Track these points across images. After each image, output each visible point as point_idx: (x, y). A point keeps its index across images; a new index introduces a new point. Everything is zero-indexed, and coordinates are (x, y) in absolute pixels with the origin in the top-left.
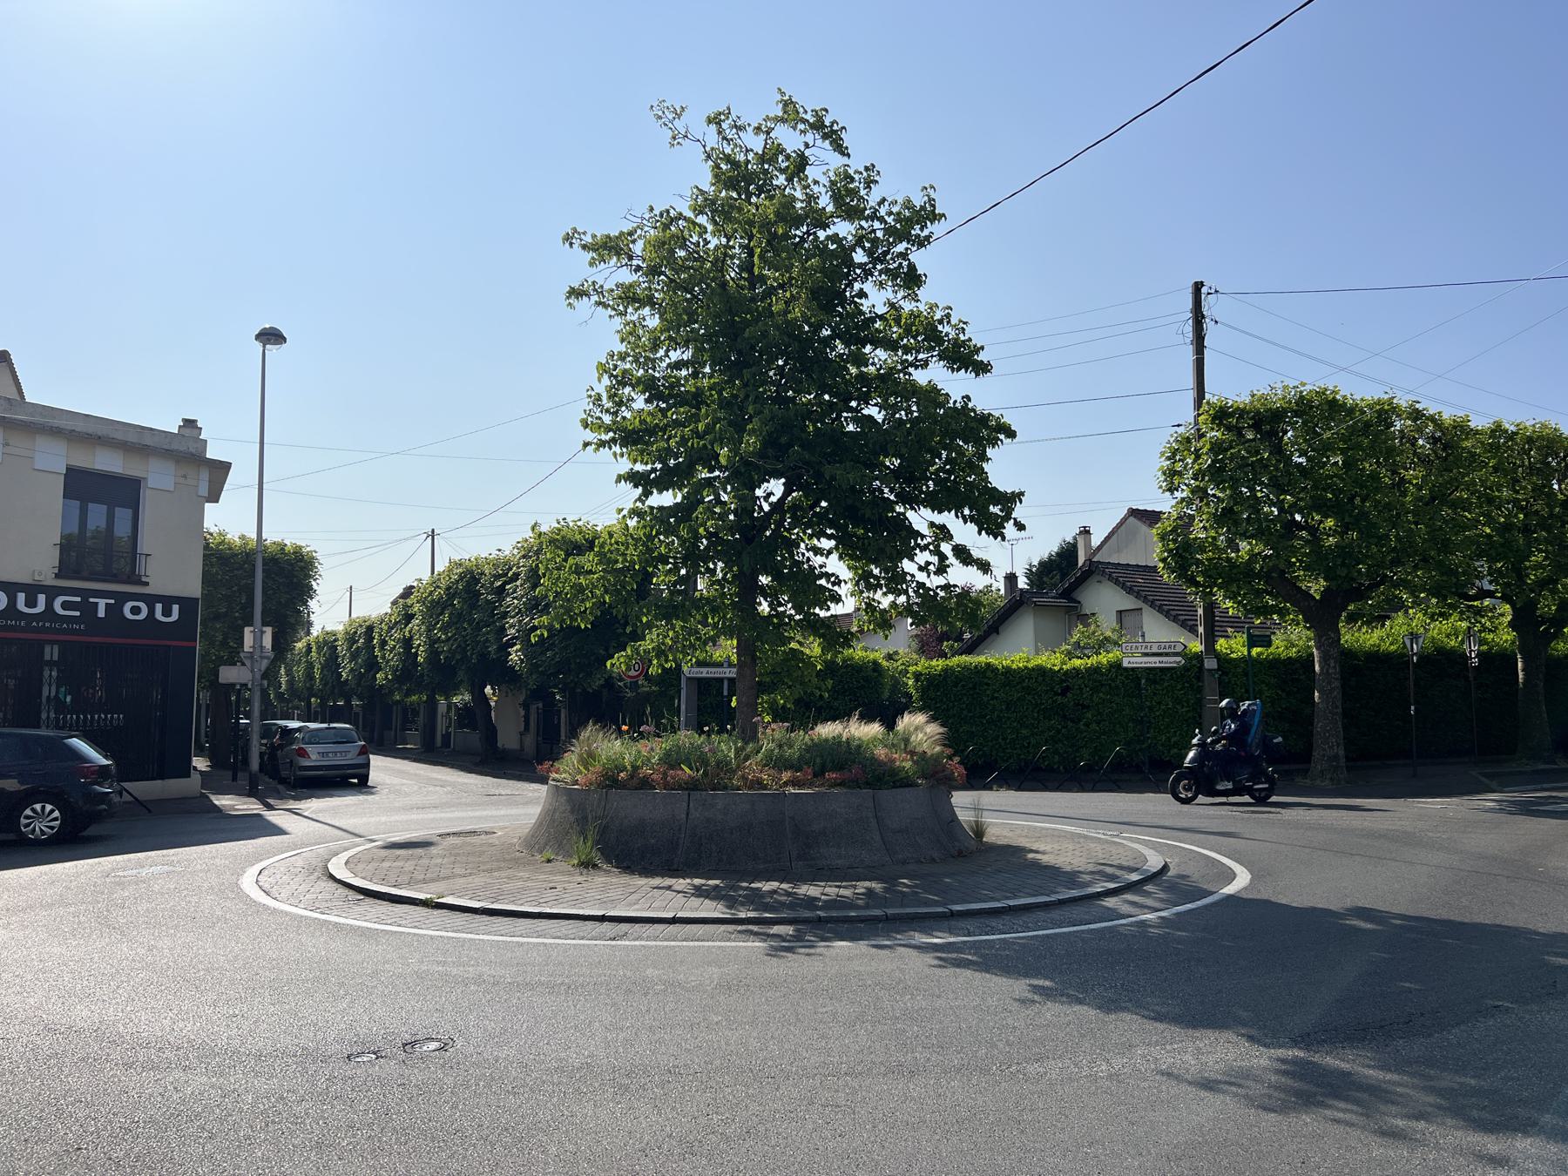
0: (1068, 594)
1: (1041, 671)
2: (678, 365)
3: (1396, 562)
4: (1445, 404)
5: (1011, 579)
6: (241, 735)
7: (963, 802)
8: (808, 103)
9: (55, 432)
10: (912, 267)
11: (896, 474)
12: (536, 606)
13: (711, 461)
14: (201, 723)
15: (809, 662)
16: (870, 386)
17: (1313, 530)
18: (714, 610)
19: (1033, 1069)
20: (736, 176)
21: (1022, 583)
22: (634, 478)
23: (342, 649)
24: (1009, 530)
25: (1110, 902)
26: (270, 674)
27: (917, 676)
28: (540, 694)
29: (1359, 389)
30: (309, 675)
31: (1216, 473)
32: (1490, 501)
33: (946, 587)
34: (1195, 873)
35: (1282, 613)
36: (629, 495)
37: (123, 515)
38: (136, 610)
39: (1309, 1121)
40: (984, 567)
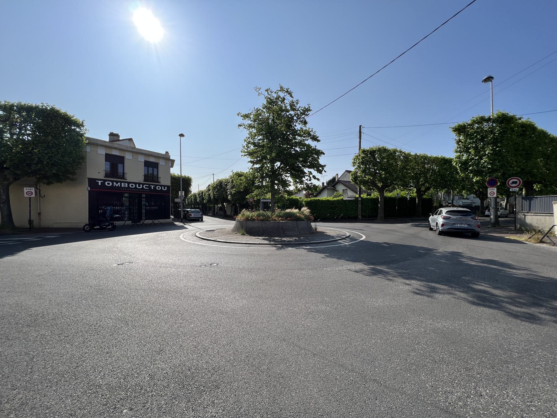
0: (334, 186)
1: (328, 200)
2: (259, 140)
3: (395, 180)
4: (407, 150)
5: (323, 183)
6: (179, 212)
7: (313, 224)
8: (285, 87)
9: (142, 154)
10: (305, 120)
11: (302, 161)
12: (232, 188)
13: (265, 158)
14: (172, 209)
15: (285, 198)
16: (297, 144)
17: (380, 174)
18: (267, 188)
19: (325, 269)
20: (271, 102)
21: (325, 184)
22: (251, 162)
23: (197, 196)
24: (323, 172)
25: (340, 241)
26: (184, 200)
27: (305, 201)
28: (234, 205)
29: (390, 147)
30: (191, 201)
31: (362, 163)
32: (414, 169)
33: (311, 183)
34: (355, 236)
35: (374, 190)
36: (250, 165)
37: (155, 170)
38: (159, 188)
39: (375, 278)
40: (318, 180)
